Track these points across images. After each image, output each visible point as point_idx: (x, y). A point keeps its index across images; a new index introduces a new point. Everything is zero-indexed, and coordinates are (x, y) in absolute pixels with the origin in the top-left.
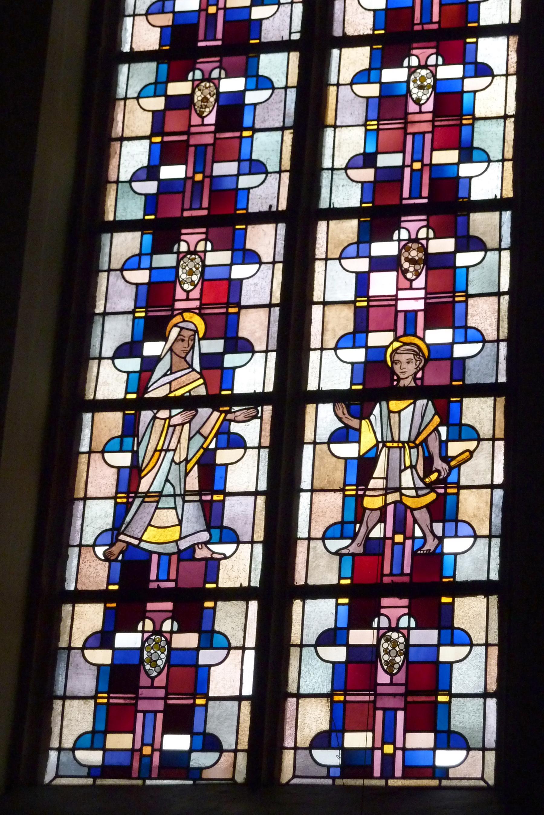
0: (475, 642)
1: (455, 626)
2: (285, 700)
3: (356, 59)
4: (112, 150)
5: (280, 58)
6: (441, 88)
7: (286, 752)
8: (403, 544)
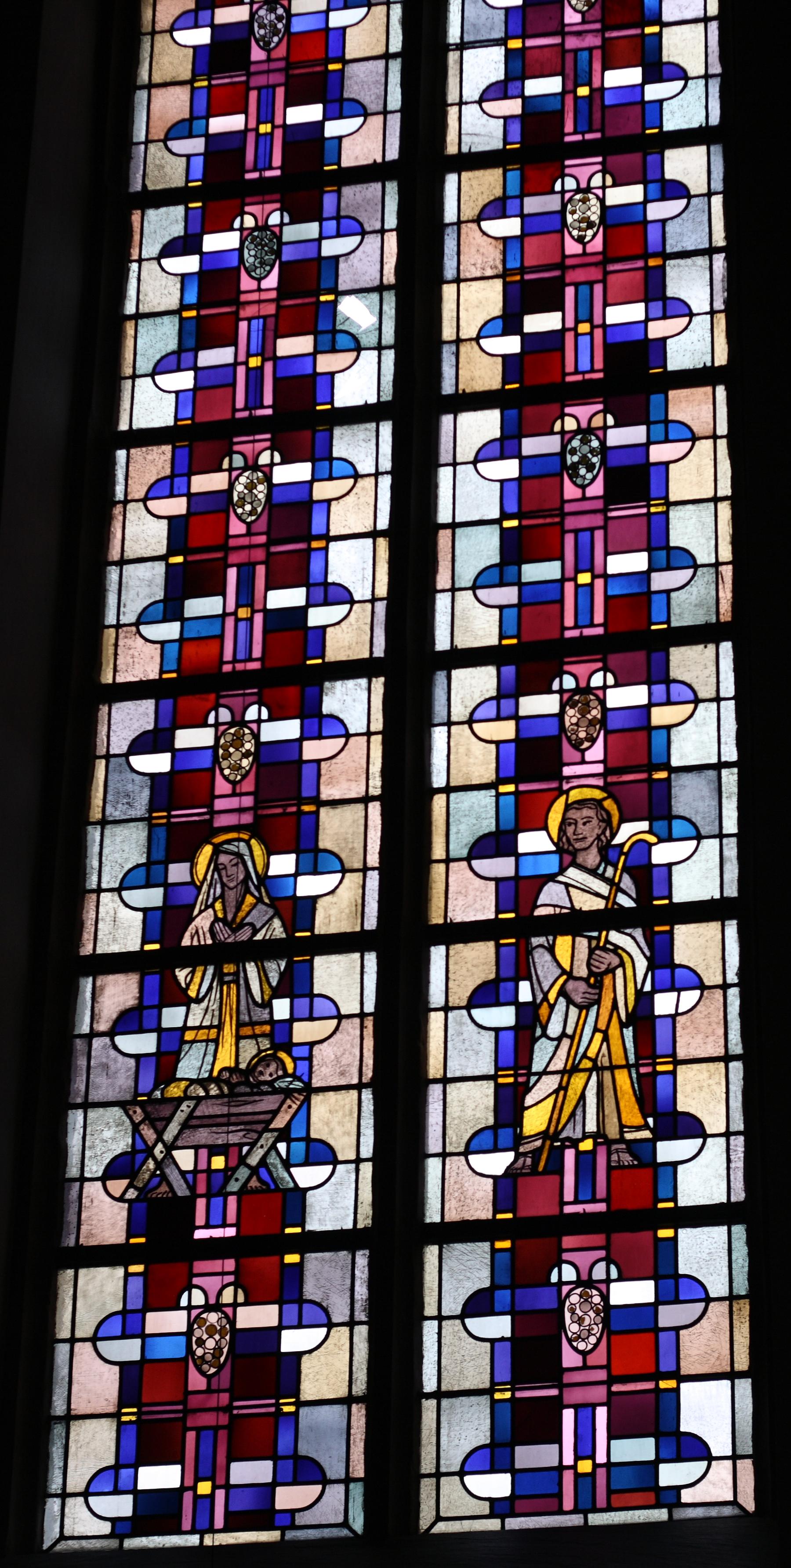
0: (695, 311)
1: (677, 961)
2: (427, 1086)
3: (481, 426)
4: (89, 837)
5: (363, 432)
6: (614, 461)
7: (433, 1015)
8: (591, 585)
